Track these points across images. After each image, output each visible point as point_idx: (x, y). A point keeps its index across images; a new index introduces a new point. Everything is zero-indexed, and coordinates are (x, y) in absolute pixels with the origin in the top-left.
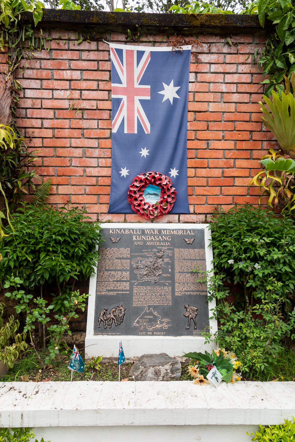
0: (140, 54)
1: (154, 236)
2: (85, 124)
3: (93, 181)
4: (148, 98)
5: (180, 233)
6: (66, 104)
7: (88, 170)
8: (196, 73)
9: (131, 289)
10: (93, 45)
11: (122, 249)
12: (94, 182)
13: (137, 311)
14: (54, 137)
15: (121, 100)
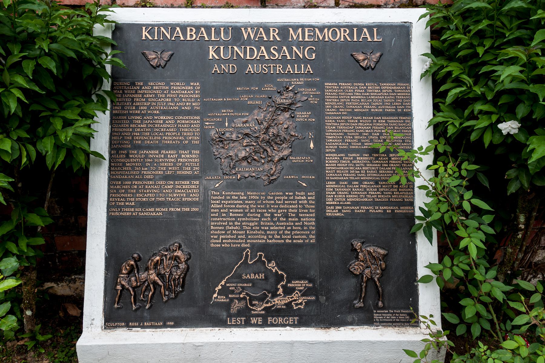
1: (268, 45)
5: (341, 35)
9: (205, 203)
11: (178, 87)
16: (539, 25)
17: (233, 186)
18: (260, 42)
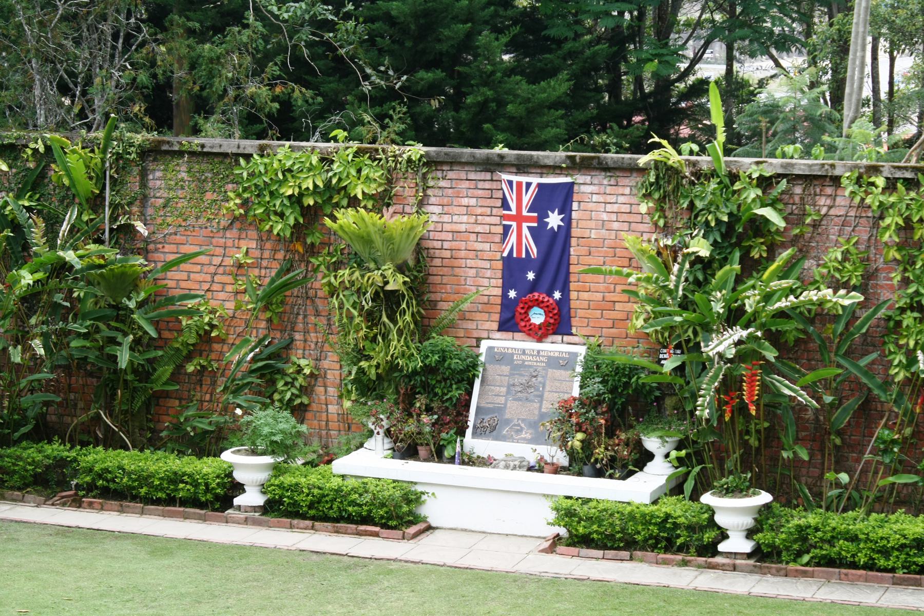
0: (529, 185)
1: (533, 356)
2: (479, 246)
3: (485, 299)
4: (535, 225)
5: (557, 354)
6: (463, 228)
7: (481, 289)
8: (580, 202)
9: (505, 404)
10: (488, 176)
11: (503, 367)
12: (486, 301)
13: (507, 422)
14: (452, 257)
15: (510, 226)
16: (919, 245)
17: (515, 400)
18: (531, 355)
